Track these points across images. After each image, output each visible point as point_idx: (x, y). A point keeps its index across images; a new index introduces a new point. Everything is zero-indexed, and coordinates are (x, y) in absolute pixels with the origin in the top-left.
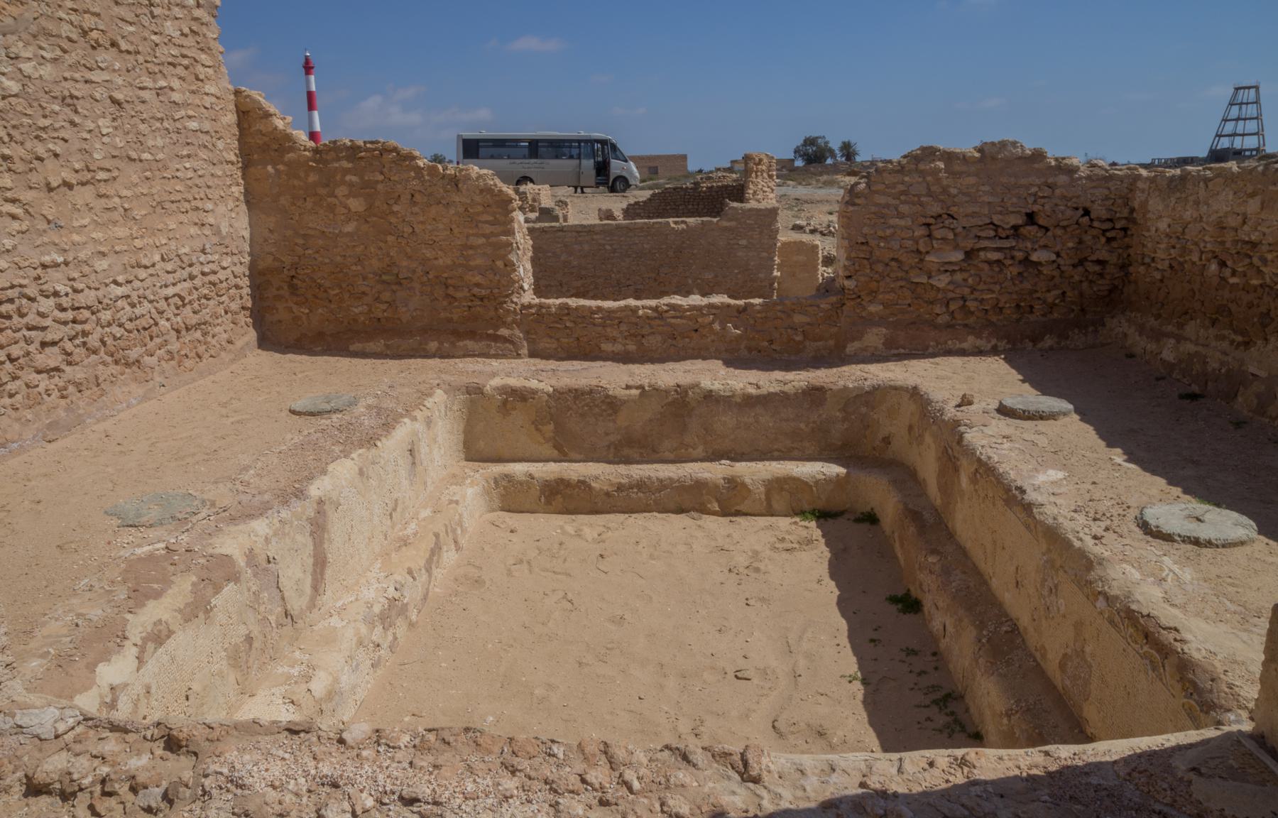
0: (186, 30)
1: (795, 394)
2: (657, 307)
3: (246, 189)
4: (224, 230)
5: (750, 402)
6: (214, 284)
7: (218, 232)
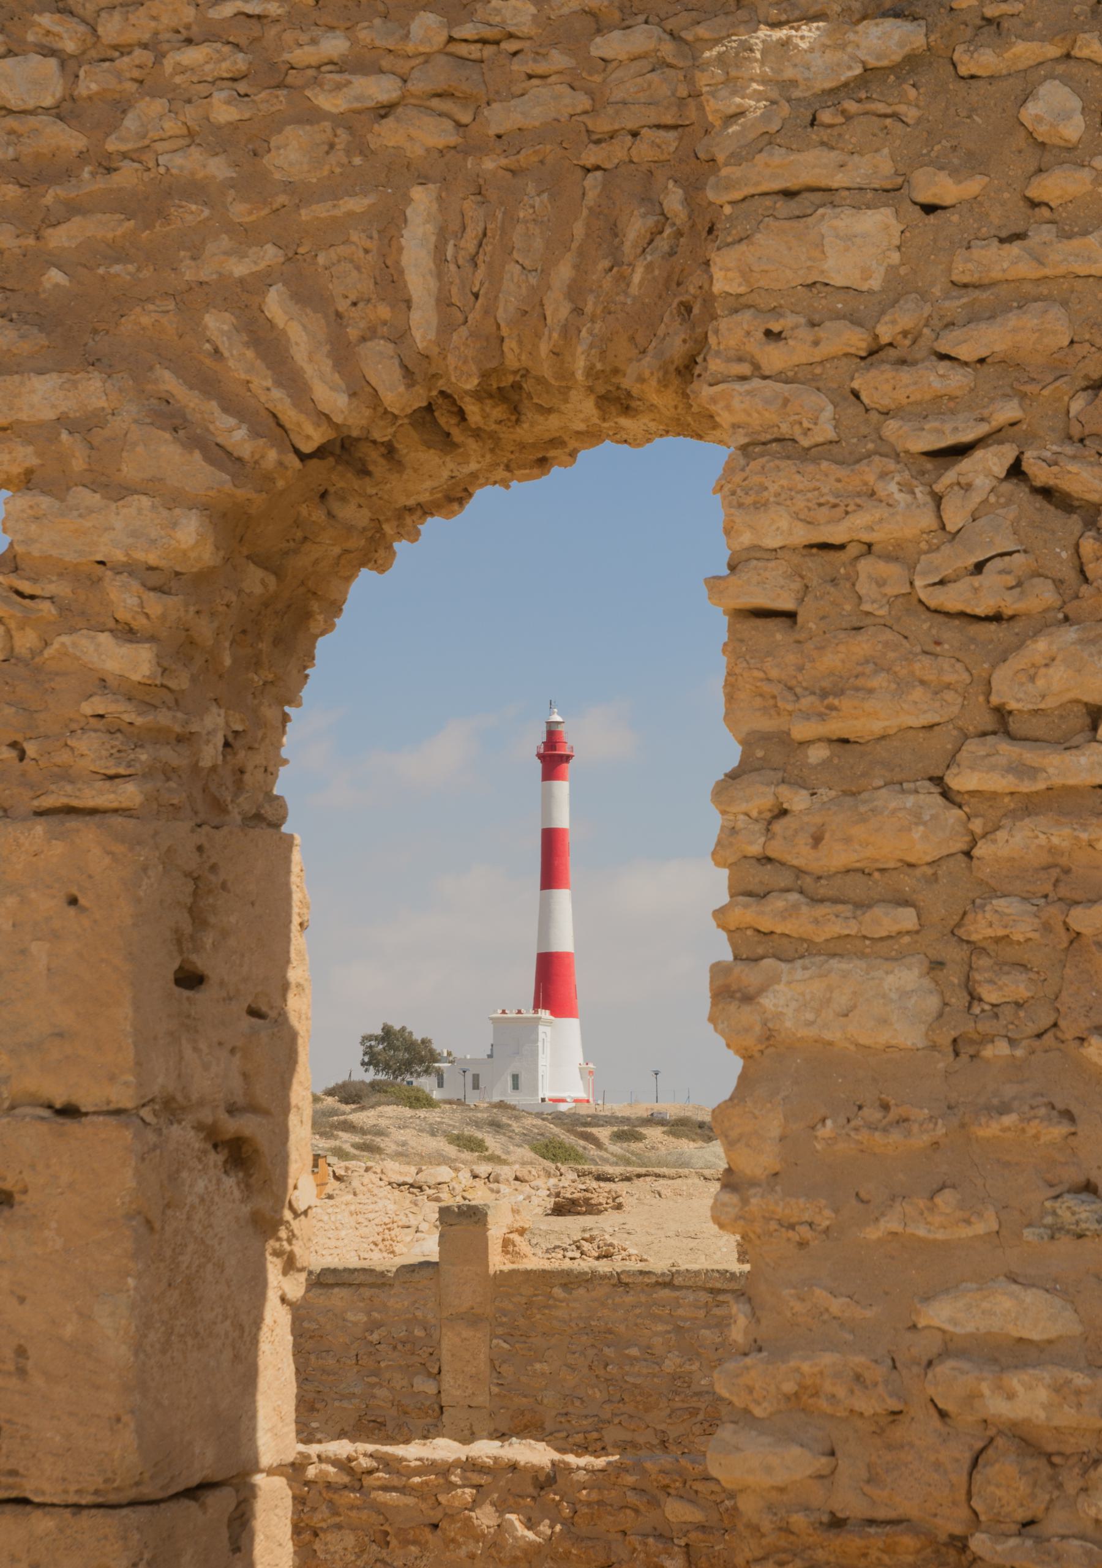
2: (350, 1459)
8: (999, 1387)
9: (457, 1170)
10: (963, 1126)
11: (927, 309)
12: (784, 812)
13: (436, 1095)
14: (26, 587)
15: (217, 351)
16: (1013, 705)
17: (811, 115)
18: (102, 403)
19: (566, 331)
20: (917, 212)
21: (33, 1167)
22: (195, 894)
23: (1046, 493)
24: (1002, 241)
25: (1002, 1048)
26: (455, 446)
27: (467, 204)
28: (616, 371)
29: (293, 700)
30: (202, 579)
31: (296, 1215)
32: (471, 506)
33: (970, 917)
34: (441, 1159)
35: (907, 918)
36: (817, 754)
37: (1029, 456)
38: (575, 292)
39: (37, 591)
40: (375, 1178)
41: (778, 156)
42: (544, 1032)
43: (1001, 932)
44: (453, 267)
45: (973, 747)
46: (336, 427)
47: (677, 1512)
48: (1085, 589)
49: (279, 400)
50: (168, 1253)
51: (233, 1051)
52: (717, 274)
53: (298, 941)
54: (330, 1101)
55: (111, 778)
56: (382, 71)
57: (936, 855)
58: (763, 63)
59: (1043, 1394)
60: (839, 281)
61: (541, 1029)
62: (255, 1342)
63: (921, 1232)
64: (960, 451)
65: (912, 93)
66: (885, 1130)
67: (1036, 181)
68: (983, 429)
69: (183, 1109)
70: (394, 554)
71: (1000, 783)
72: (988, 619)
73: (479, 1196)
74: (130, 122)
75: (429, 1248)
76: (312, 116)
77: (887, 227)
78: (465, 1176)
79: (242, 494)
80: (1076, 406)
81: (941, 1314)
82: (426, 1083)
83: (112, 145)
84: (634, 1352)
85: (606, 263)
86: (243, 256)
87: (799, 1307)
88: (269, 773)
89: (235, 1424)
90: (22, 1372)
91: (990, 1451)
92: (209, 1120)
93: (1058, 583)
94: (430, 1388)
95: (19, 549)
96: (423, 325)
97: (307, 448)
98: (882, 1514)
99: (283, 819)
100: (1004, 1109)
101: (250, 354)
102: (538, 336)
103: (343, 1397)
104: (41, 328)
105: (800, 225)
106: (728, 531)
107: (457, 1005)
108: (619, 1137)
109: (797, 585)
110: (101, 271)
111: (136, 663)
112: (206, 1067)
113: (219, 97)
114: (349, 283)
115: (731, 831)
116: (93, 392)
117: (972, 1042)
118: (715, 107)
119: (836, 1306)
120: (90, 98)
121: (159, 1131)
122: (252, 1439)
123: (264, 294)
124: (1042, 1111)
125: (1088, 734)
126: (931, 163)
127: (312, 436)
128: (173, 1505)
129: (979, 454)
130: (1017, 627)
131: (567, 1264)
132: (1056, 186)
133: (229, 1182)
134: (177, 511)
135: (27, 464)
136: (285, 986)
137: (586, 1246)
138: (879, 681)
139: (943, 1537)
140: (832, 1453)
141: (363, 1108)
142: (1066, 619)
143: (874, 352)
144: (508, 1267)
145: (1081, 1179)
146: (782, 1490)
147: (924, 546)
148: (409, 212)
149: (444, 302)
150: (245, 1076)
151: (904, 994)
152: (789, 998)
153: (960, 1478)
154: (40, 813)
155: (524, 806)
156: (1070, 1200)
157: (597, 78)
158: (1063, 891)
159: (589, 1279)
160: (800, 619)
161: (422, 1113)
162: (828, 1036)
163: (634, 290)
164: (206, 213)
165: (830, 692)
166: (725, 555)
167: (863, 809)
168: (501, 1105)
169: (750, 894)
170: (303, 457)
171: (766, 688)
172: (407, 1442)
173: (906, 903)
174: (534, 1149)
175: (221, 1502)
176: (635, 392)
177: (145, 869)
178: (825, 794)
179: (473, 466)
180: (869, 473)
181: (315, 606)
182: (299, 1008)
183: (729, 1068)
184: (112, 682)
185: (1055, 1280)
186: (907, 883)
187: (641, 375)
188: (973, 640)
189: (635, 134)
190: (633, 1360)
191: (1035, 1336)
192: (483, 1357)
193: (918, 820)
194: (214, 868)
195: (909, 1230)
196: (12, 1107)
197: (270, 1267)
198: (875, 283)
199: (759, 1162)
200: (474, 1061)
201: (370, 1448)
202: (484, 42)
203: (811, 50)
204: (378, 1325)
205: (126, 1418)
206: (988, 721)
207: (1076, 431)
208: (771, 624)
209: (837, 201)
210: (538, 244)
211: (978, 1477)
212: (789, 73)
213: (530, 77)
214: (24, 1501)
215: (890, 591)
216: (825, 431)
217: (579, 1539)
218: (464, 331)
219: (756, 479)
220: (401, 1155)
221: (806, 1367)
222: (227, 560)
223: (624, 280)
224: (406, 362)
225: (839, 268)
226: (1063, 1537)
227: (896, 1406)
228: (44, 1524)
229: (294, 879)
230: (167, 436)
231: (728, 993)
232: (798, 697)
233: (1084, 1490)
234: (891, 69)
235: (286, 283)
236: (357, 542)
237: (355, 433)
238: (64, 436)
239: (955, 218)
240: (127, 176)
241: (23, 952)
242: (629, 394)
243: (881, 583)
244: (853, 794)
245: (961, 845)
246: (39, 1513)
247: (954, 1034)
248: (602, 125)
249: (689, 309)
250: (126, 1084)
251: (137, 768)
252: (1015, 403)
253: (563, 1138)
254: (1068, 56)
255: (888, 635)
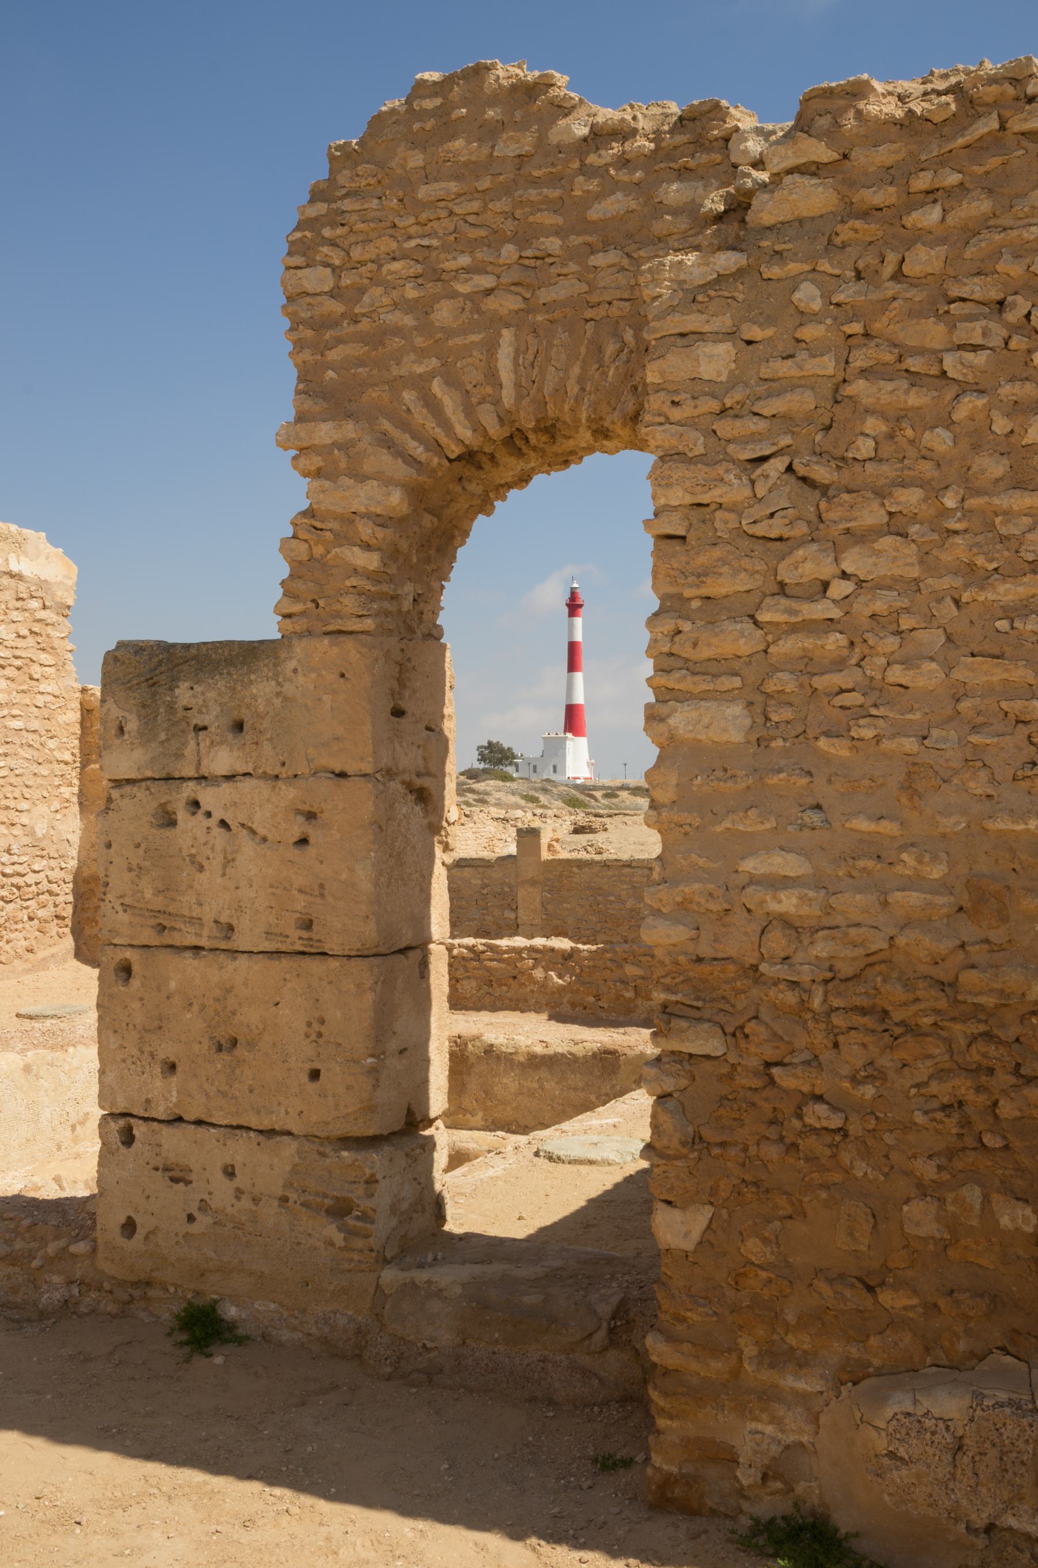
0: (25, 632)
1: (585, 1057)
2: (474, 946)
3: (80, 791)
4: (40, 832)
5: (537, 1063)
6: (19, 888)
7: (32, 833)
8: (774, 898)
9: (525, 812)
10: (761, 779)
11: (748, 391)
12: (680, 632)
13: (515, 775)
14: (318, 525)
15: (409, 409)
16: (787, 581)
17: (693, 297)
18: (354, 435)
19: (578, 400)
20: (744, 344)
21: (326, 801)
22: (400, 672)
23: (804, 479)
24: (783, 358)
25: (780, 742)
26: (524, 454)
27: (529, 338)
28: (601, 418)
29: (446, 578)
30: (403, 520)
31: (449, 824)
32: (532, 483)
33: (766, 681)
34: (517, 807)
35: (737, 682)
36: (695, 604)
37: (796, 461)
38: (581, 380)
39: (324, 527)
40: (485, 815)
41: (677, 317)
42: (569, 744)
43: (780, 688)
44: (522, 368)
45: (768, 601)
46: (467, 446)
47: (631, 970)
48: (821, 526)
49: (439, 433)
50: (389, 841)
51: (419, 747)
52: (649, 374)
53: (449, 695)
54: (462, 777)
55: (360, 616)
56: (487, 273)
57: (751, 652)
58: (670, 272)
59: (794, 901)
60: (706, 377)
61: (568, 742)
62: (430, 883)
63: (741, 828)
64: (764, 459)
65: (741, 287)
66: (725, 781)
67: (799, 330)
68: (774, 449)
69: (396, 774)
70: (494, 507)
71: (780, 617)
72: (776, 540)
73: (536, 824)
74: (366, 299)
75: (512, 849)
76: (454, 295)
77: (729, 352)
78: (529, 815)
79: (421, 479)
80: (818, 438)
81: (749, 865)
82: (510, 770)
83: (358, 310)
84: (612, 898)
85: (596, 366)
86: (421, 363)
87: (684, 862)
88: (435, 614)
89: (422, 921)
90: (322, 895)
91: (770, 927)
92: (408, 779)
93: (809, 523)
94: (512, 916)
95: (315, 506)
96: (508, 396)
97: (453, 456)
98: (720, 955)
99: (441, 636)
100: (780, 771)
101: (425, 411)
102: (564, 402)
103: (469, 920)
104: (324, 399)
105: (688, 350)
106: (654, 497)
107: (526, 727)
108: (606, 796)
109: (686, 523)
110: (353, 371)
111: (371, 561)
112: (406, 755)
113: (409, 286)
114: (472, 376)
115: (654, 641)
116: (350, 430)
117: (766, 740)
118: (647, 293)
119: (701, 862)
120: (347, 287)
121: (384, 785)
122: (429, 928)
123: (431, 382)
124: (797, 772)
125: (821, 595)
126: (749, 321)
127: (455, 451)
128: (393, 957)
129: (772, 461)
130: (790, 543)
131: (579, 856)
132: (810, 332)
133: (418, 809)
134: (390, 488)
135: (318, 465)
136: (443, 716)
137: (589, 849)
138: (725, 569)
139: (747, 966)
140: (698, 929)
141: (478, 782)
142: (813, 540)
143: (723, 411)
144: (551, 857)
145: (815, 803)
146: (674, 945)
147: (746, 505)
148: (501, 341)
149: (518, 385)
150: (425, 759)
151: (735, 718)
152: (681, 719)
153: (756, 939)
154: (326, 634)
155: (560, 631)
156: (809, 813)
157: (592, 276)
158: (809, 669)
159: (590, 863)
160: (688, 540)
161: (508, 784)
162: (699, 737)
163: (610, 379)
164: (403, 342)
165: (702, 575)
166: (652, 509)
167: (716, 630)
168: (548, 780)
169: (663, 671)
170: (450, 461)
171: (672, 573)
172: (502, 938)
173: (737, 675)
174: (564, 802)
175: (414, 956)
176: (610, 428)
177: (376, 660)
178: (699, 623)
179: (533, 464)
180: (720, 470)
181: (457, 533)
182: (449, 727)
183: (652, 753)
184: (360, 570)
185: (802, 849)
186: (737, 665)
187: (613, 420)
188: (769, 550)
189: (610, 303)
190: (612, 902)
191: (792, 875)
192: (538, 901)
193: (743, 636)
194: (409, 660)
195: (736, 827)
196: (315, 773)
197: (436, 849)
198: (723, 378)
199: (665, 796)
200: (534, 759)
201: (484, 941)
202: (537, 258)
203: (693, 266)
204: (487, 886)
205: (371, 917)
206: (775, 588)
207: (818, 450)
208: (674, 542)
209: (705, 338)
210: (563, 356)
211: (764, 938)
212: (682, 277)
213: (559, 275)
214: (325, 954)
215: (730, 526)
216: (700, 449)
217: (583, 983)
218: (528, 399)
219: (667, 473)
220: (498, 805)
221: (687, 890)
222: (414, 511)
223: (605, 374)
224: (500, 414)
225: (707, 371)
226: (801, 964)
227: (726, 906)
228: (334, 964)
229: (447, 665)
230: (385, 451)
231: (653, 717)
232: (686, 577)
233: (812, 943)
234: (731, 275)
235: (442, 376)
236: (477, 502)
237: (475, 449)
238: (336, 451)
239: (761, 347)
240: (365, 325)
241: (319, 699)
242: (608, 430)
243: (726, 522)
244: (712, 623)
245: (762, 647)
246: (331, 959)
247: (758, 736)
248: (594, 299)
249: (636, 389)
250: (369, 762)
251: (372, 612)
252: (789, 436)
253: (579, 796)
254: (814, 270)
255: (729, 547)
